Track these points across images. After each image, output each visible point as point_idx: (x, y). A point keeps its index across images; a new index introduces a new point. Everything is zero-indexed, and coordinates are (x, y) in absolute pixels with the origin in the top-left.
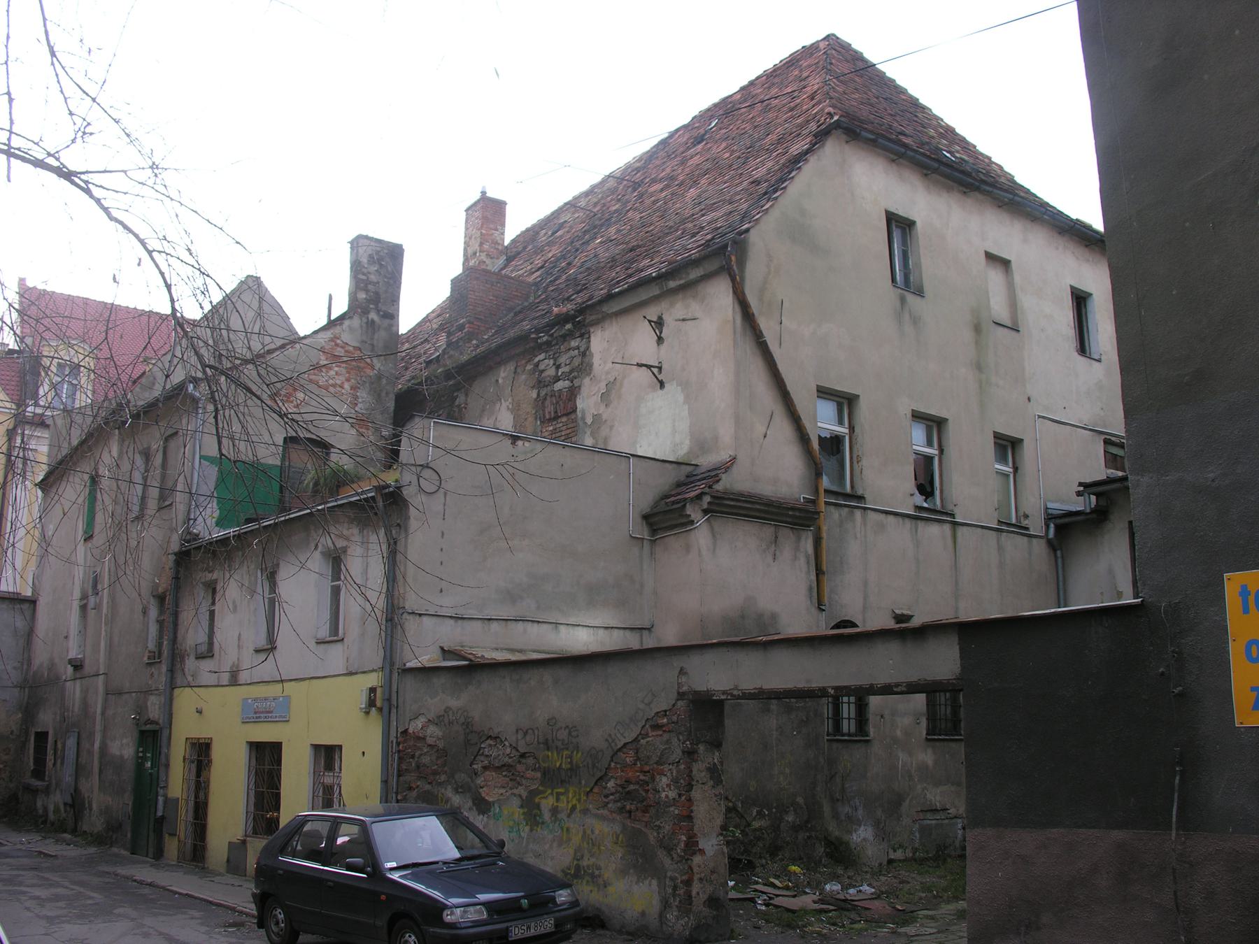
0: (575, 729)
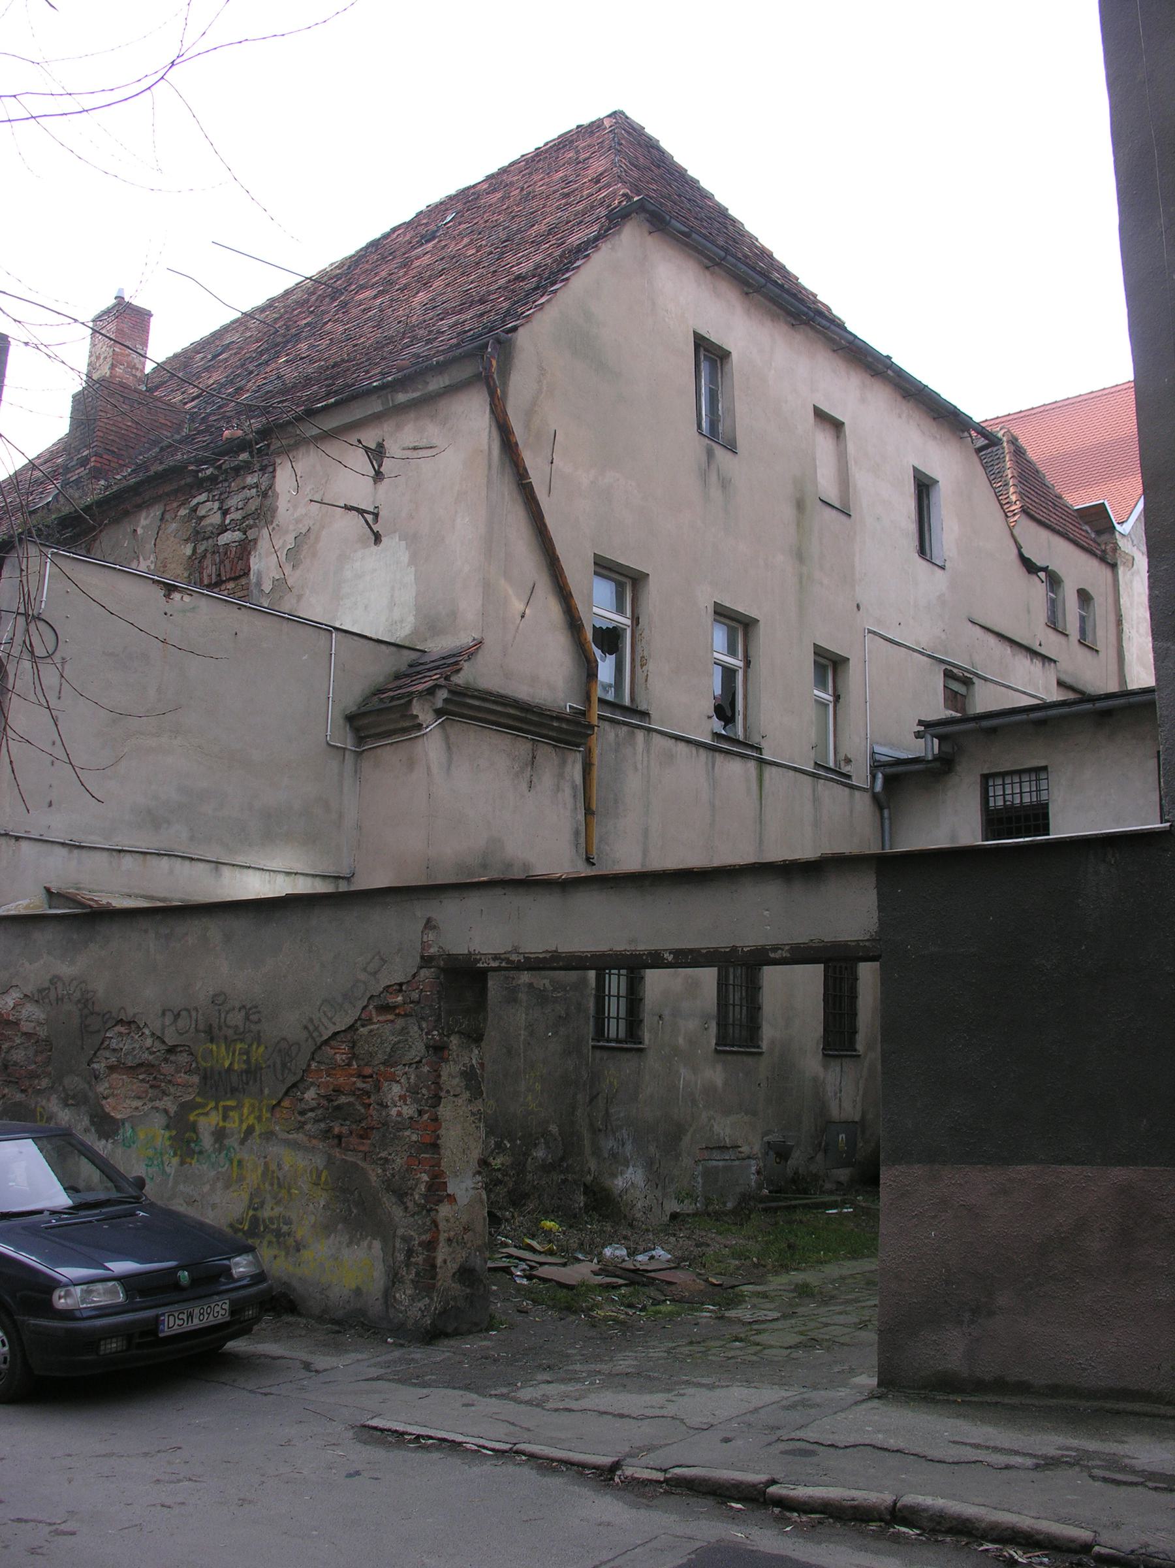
0: (254, 1010)
